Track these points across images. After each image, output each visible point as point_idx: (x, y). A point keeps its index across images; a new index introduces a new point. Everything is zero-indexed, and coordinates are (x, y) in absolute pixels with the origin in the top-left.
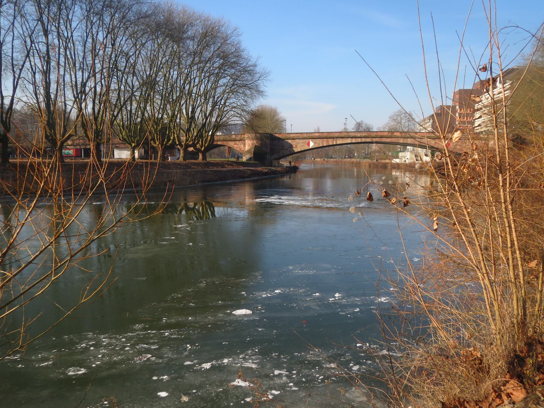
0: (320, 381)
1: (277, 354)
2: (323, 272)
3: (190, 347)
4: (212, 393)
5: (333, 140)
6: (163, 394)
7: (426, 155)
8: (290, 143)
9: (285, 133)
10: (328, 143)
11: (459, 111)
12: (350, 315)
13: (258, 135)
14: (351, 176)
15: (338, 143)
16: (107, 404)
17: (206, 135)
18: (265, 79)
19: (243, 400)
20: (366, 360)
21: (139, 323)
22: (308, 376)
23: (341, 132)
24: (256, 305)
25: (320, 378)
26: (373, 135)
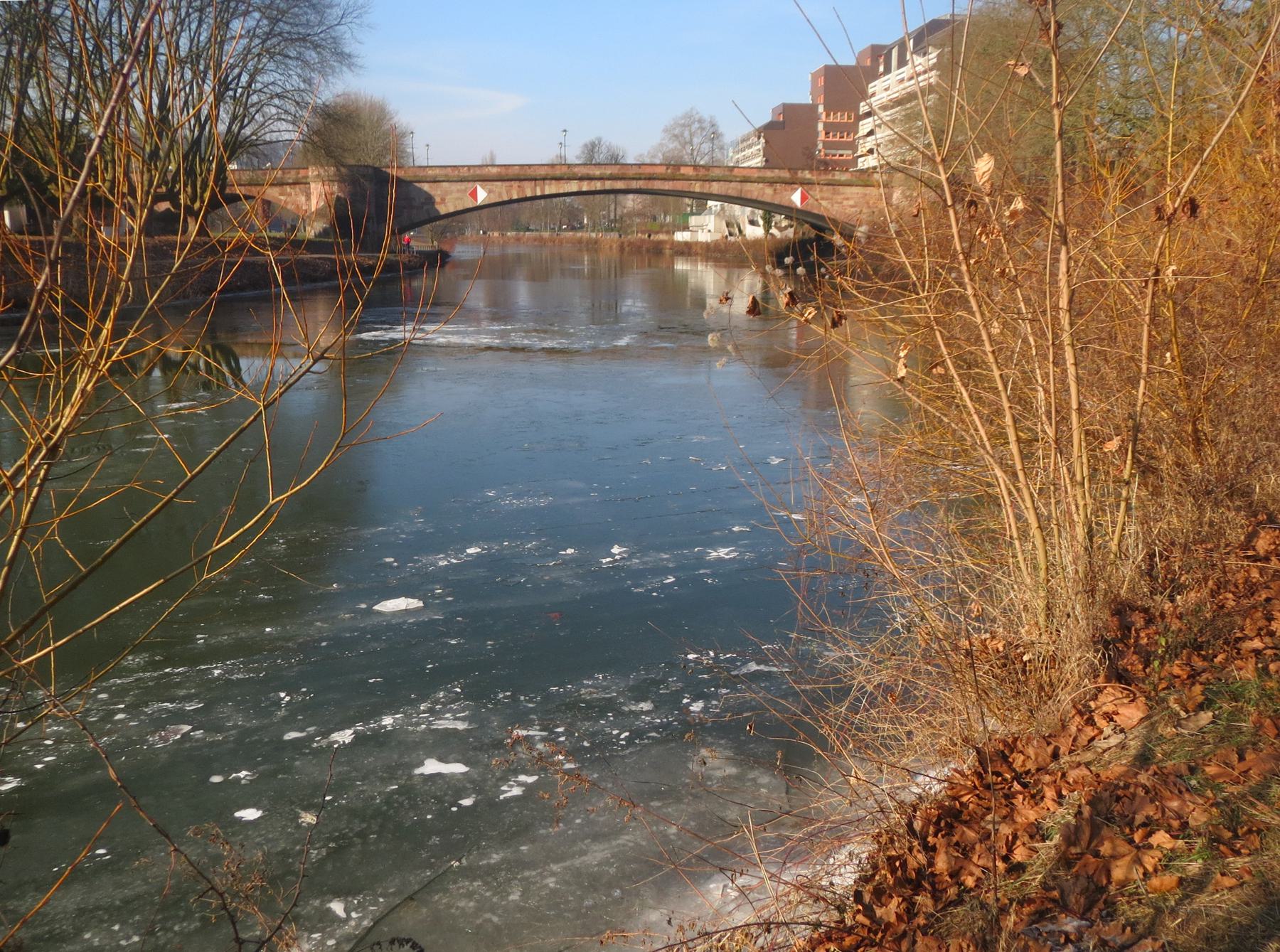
0: (624, 743)
1: (508, 694)
2: (572, 501)
3: (288, 699)
4: (374, 798)
5: (536, 185)
6: (250, 814)
7: (752, 223)
8: (426, 192)
9: (414, 167)
10: (523, 191)
11: (823, 116)
12: (657, 592)
13: (343, 170)
14: (577, 274)
16: (105, 855)
17: (204, 168)
18: (357, 21)
19: (455, 804)
20: (717, 687)
21: (136, 650)
22: (594, 734)
23: (552, 166)
24: (430, 587)
25: (622, 736)
26: (631, 172)
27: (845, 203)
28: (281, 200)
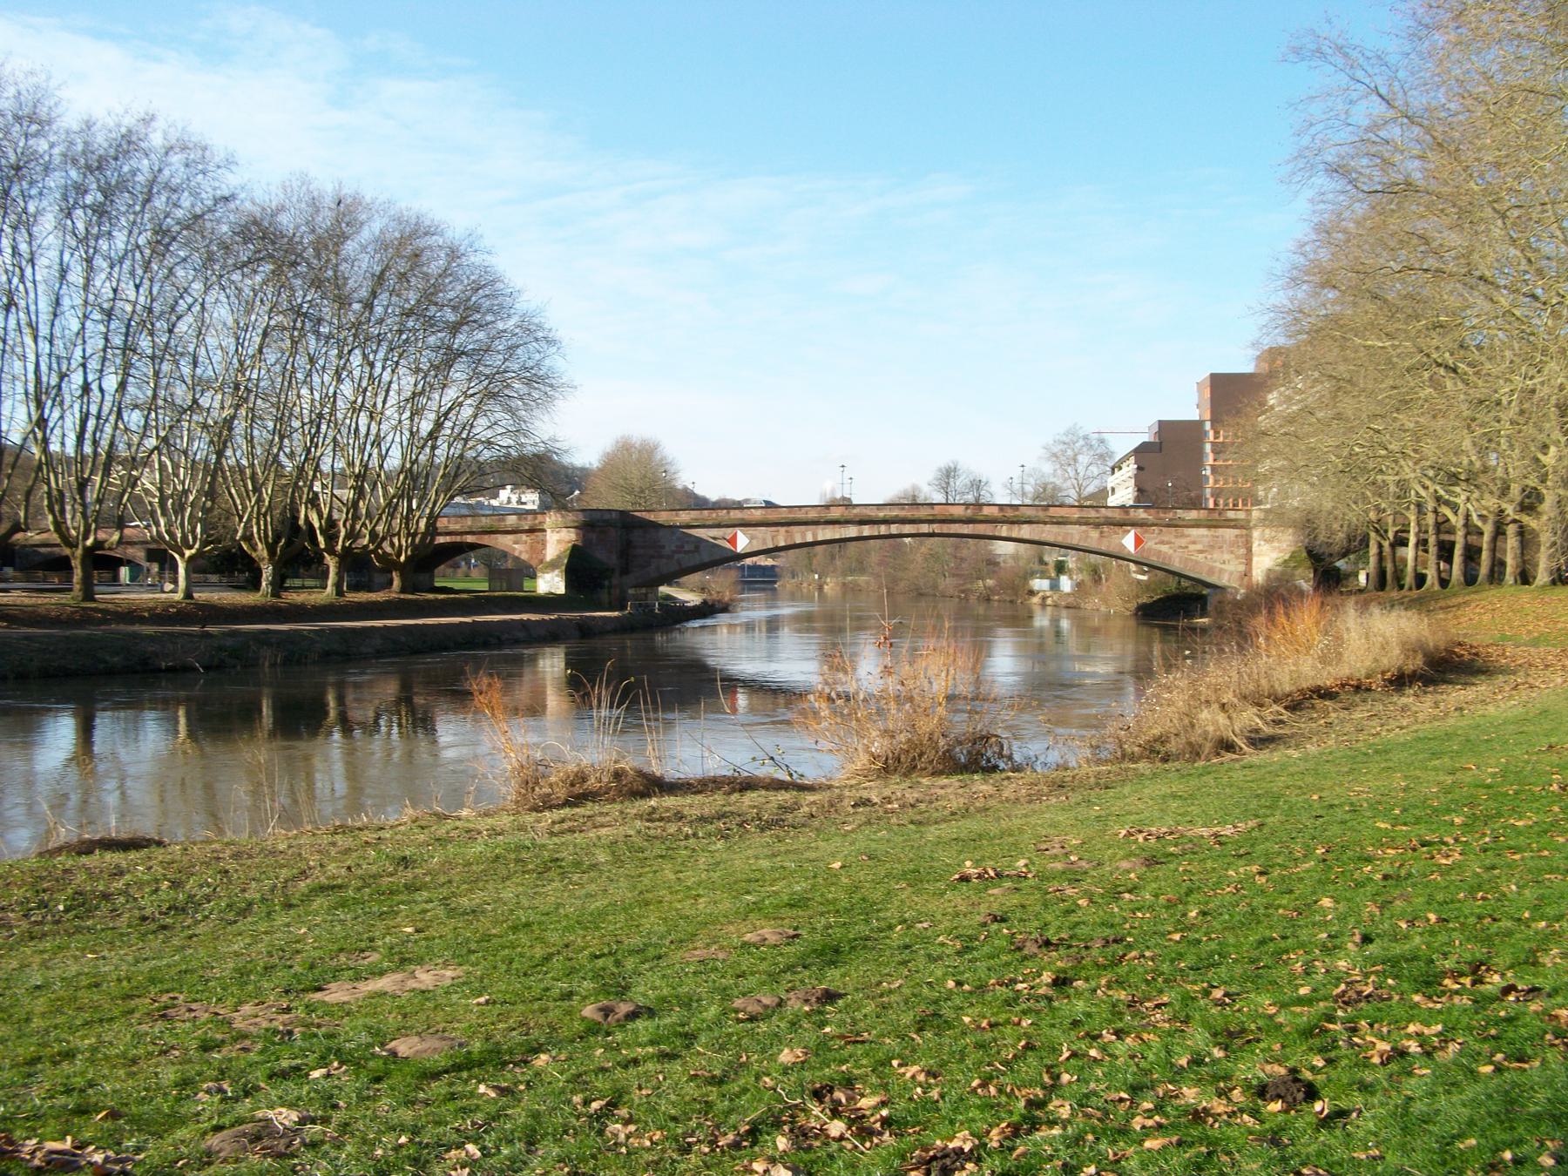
11: (1211, 434)
15: (820, 539)
27: (1192, 547)
28: (514, 549)
